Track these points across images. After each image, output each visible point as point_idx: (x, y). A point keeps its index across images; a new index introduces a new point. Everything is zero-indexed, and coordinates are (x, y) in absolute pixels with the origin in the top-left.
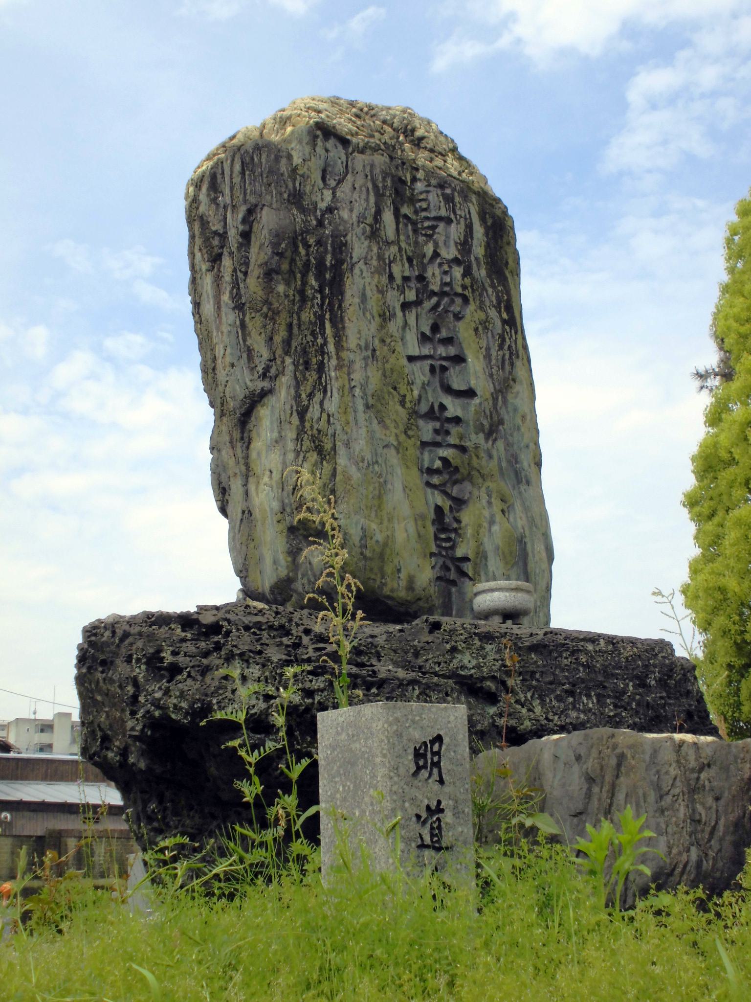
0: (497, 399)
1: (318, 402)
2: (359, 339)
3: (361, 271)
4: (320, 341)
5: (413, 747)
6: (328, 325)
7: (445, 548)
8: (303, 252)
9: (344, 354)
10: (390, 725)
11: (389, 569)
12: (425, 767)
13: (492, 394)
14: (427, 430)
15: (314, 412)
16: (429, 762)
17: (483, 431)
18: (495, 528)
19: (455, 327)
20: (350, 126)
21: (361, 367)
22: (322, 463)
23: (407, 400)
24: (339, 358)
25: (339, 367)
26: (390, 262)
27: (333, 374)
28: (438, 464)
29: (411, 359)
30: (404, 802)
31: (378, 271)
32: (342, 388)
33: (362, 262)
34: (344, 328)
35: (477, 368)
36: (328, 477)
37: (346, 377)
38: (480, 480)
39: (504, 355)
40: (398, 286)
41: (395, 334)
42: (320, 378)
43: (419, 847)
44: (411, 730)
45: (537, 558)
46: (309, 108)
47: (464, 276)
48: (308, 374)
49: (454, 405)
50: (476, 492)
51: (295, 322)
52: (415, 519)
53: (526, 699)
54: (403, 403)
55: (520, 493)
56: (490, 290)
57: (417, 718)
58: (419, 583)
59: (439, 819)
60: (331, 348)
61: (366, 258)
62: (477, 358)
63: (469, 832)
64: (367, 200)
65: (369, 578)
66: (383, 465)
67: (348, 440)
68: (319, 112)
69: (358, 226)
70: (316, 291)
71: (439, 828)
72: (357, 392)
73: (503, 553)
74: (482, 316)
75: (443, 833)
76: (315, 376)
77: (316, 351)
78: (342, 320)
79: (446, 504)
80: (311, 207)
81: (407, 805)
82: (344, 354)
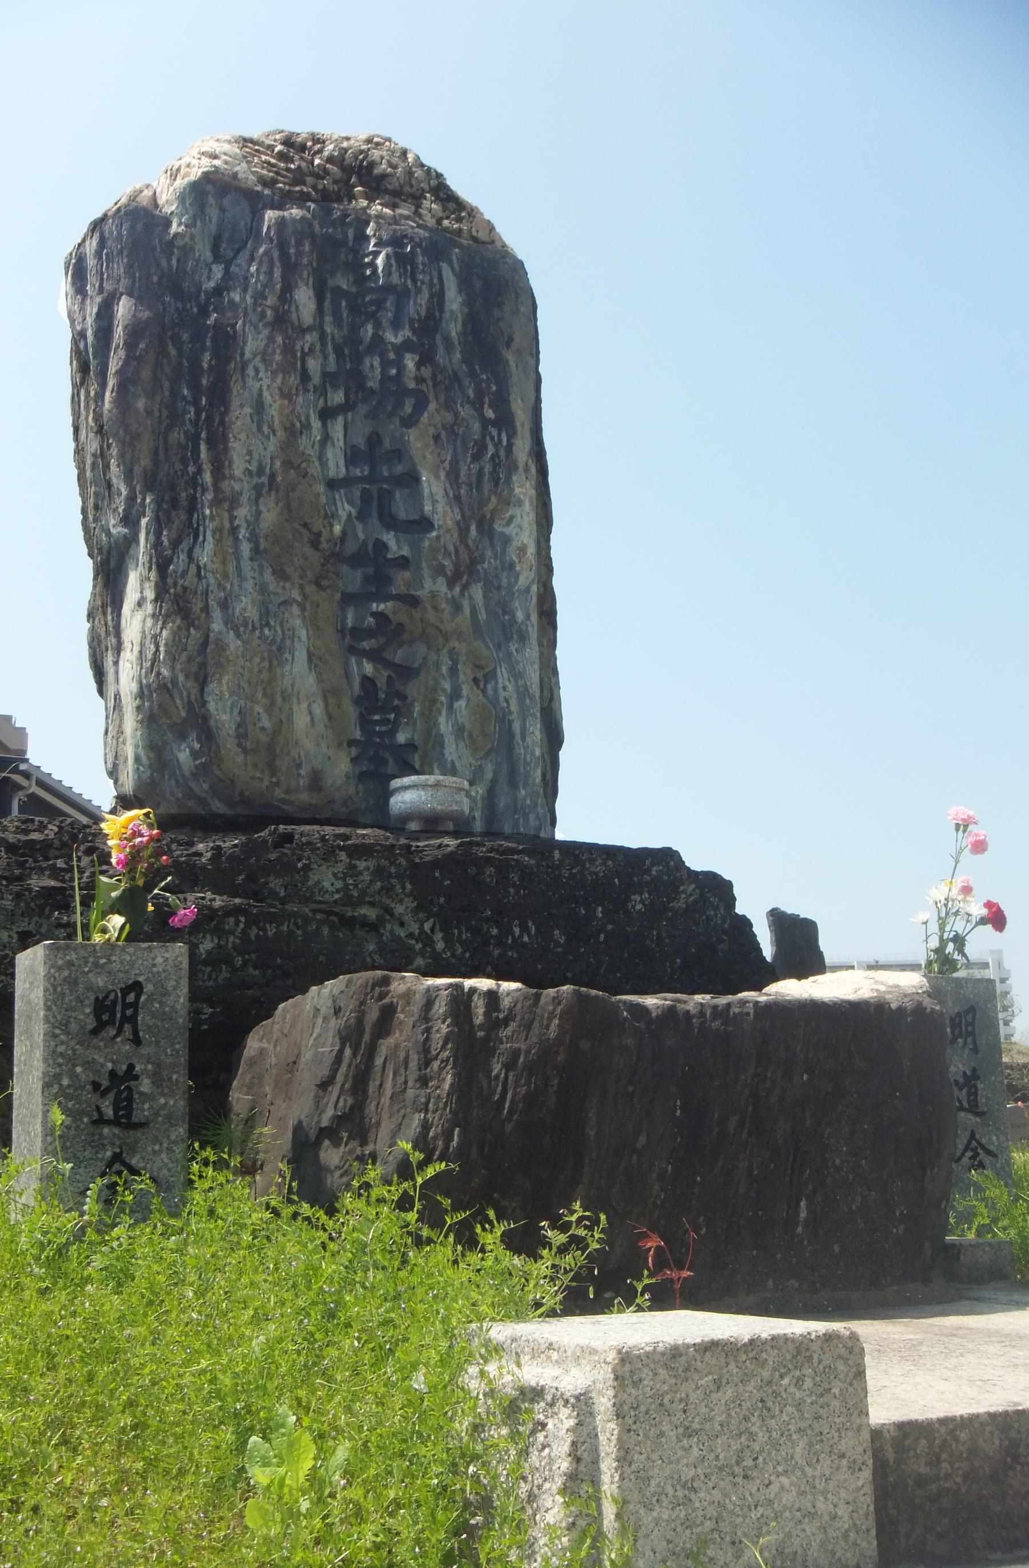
0: (468, 528)
1: (186, 549)
2: (249, 462)
3: (257, 370)
4: (191, 469)
5: (93, 997)
6: (203, 447)
7: (380, 734)
8: (173, 352)
9: (225, 485)
10: (60, 969)
11: (283, 764)
12: (111, 1022)
13: (458, 523)
14: (353, 579)
15: (181, 560)
16: (119, 1015)
17: (445, 575)
18: (461, 704)
19: (402, 435)
20: (271, 174)
21: (249, 499)
22: (188, 629)
23: (322, 539)
24: (217, 489)
25: (216, 503)
26: (304, 355)
27: (208, 512)
28: (370, 621)
29: (332, 484)
30: (74, 1066)
31: (285, 369)
32: (220, 530)
33: (258, 359)
34: (226, 449)
35: (435, 489)
36: (196, 648)
37: (226, 514)
38: (441, 640)
39: (481, 469)
40: (315, 386)
41: (310, 451)
42: (191, 516)
43: (94, 1123)
44: (90, 975)
45: (529, 740)
46: (203, 154)
47: (419, 365)
48: (174, 513)
49: (398, 541)
50: (433, 657)
51: (161, 446)
52: (325, 698)
53: (422, 931)
54: (315, 544)
55: (510, 655)
56: (466, 381)
57: (103, 961)
58: (329, 782)
59: (129, 1089)
60: (207, 477)
61: (264, 353)
62: (437, 476)
63: (178, 1104)
64: (270, 273)
65: (253, 778)
66: (278, 629)
67: (226, 598)
68: (215, 157)
69: (255, 310)
70: (188, 403)
71: (130, 1099)
72: (243, 533)
73: (470, 735)
74: (449, 417)
75: (135, 1106)
76: (184, 517)
77: (186, 482)
78: (225, 439)
79: (382, 677)
80: (192, 290)
81: (79, 1069)
82: (225, 485)
